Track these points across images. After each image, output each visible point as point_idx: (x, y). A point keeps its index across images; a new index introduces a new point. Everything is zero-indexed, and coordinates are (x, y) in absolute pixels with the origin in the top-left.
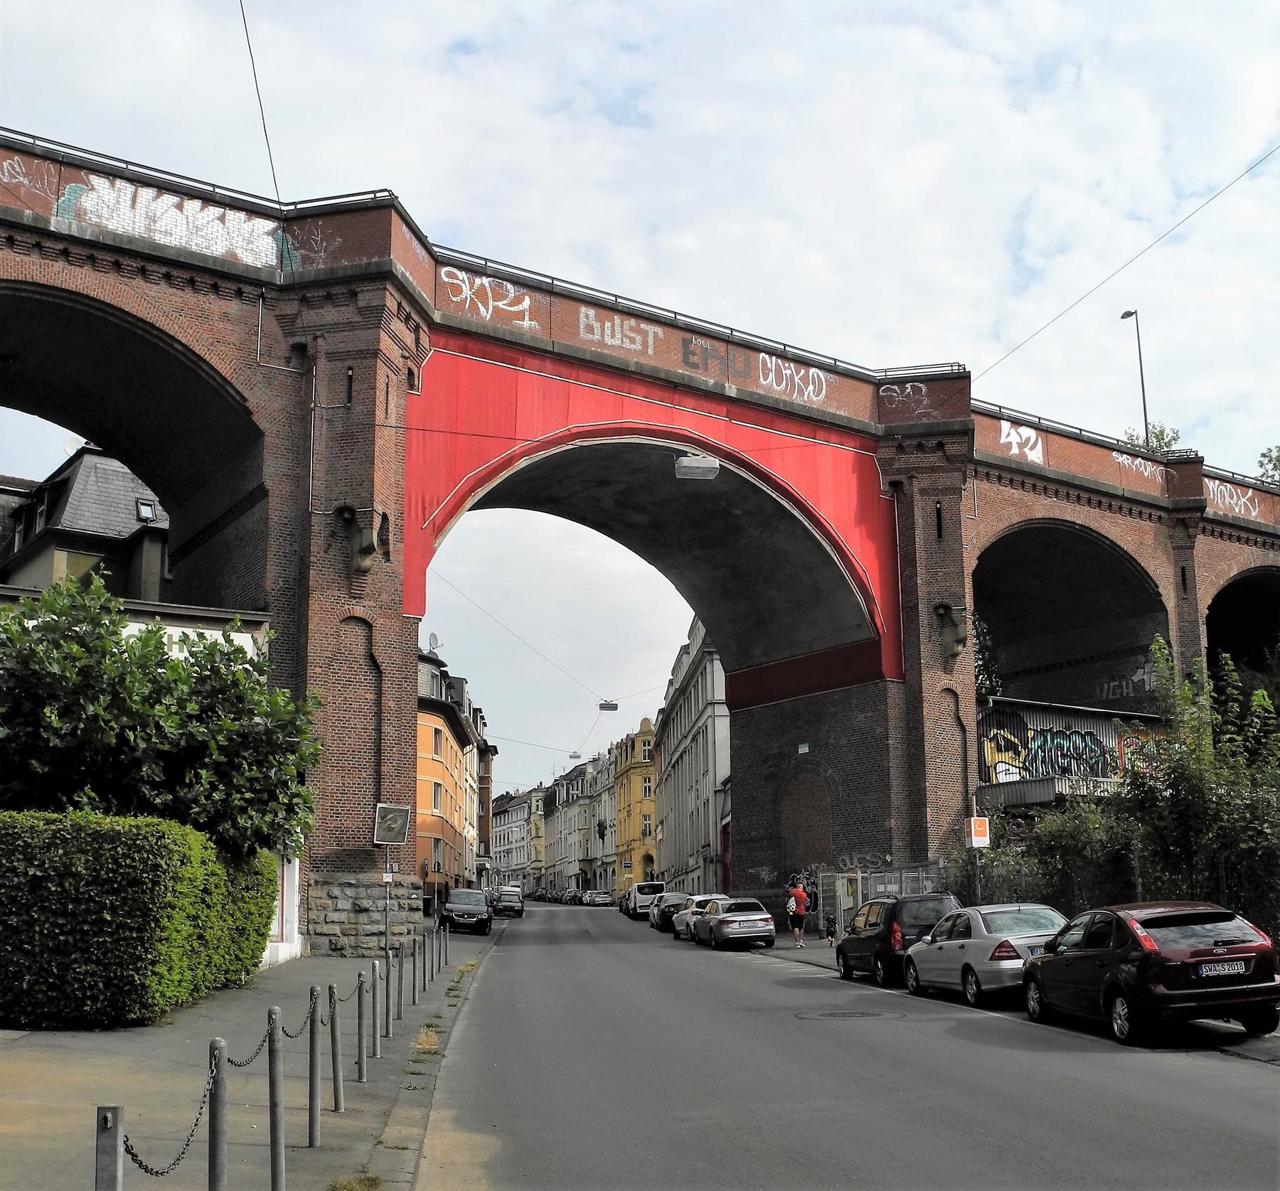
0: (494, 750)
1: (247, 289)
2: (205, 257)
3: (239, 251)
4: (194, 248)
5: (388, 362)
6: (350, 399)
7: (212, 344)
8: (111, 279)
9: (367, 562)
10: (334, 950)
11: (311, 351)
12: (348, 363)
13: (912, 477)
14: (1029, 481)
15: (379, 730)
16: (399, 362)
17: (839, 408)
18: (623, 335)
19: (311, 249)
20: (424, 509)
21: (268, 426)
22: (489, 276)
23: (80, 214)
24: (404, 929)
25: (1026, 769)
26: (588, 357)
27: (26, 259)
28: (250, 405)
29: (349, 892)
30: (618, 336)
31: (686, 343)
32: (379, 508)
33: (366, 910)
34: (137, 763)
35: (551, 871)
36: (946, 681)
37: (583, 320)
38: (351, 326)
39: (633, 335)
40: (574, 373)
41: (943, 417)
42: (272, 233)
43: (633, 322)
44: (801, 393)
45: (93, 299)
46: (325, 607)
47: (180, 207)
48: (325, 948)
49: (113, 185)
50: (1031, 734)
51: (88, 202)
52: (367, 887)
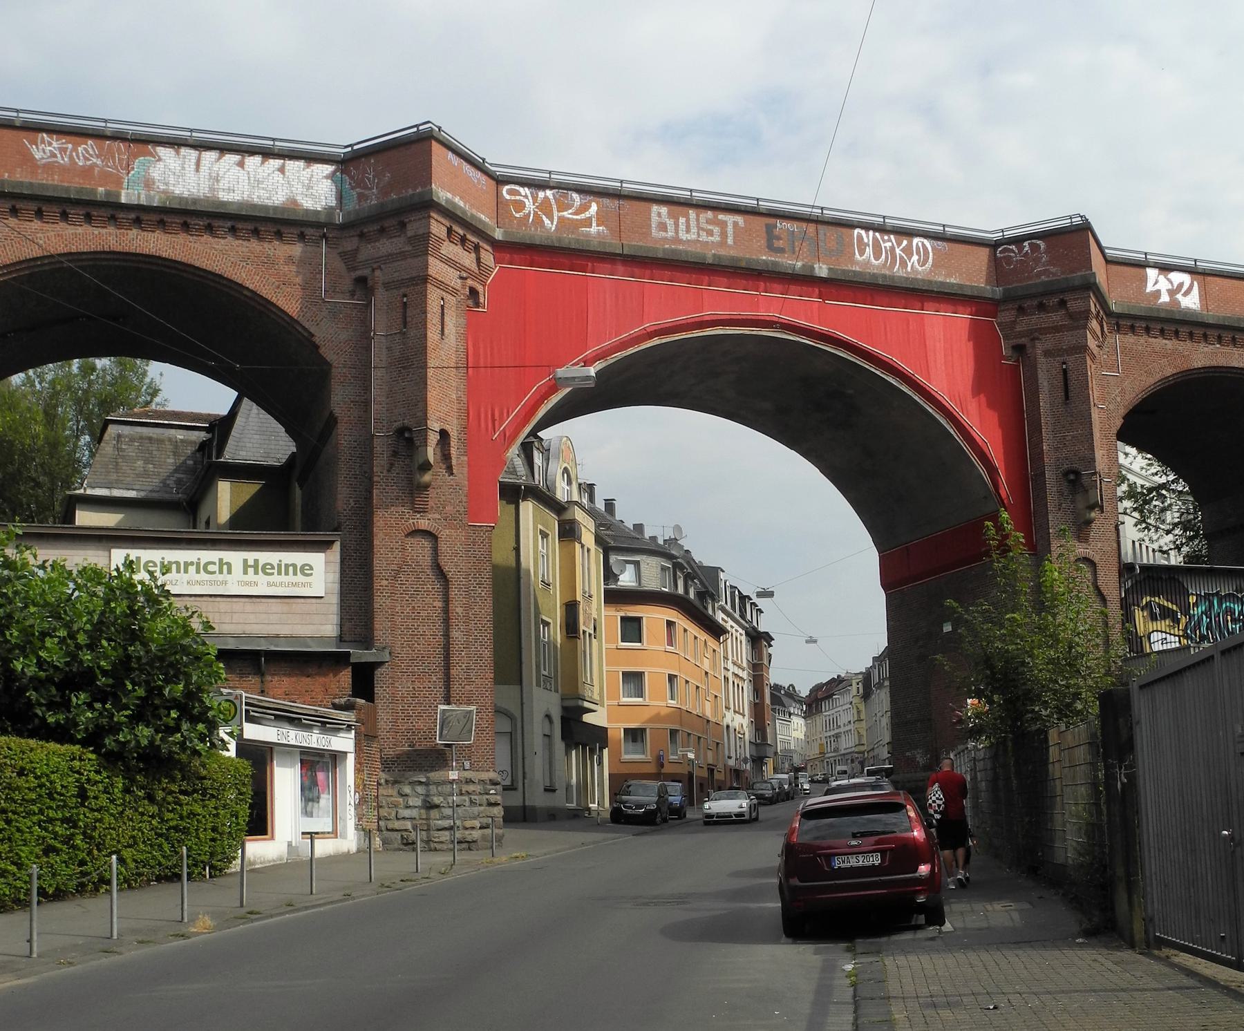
0: (768, 638)
1: (309, 231)
2: (266, 208)
3: (299, 198)
4: (256, 200)
5: (442, 285)
6: (405, 324)
7: (278, 287)
8: (182, 238)
9: (427, 478)
10: (407, 844)
11: (370, 283)
12: (403, 290)
13: (1033, 340)
14: (1184, 330)
15: (447, 635)
16: (457, 284)
17: (949, 275)
18: (699, 228)
19: (366, 188)
20: (494, 420)
21: (335, 357)
22: (552, 188)
23: (149, 184)
24: (477, 823)
25: (1187, 637)
26: (660, 255)
27: (104, 231)
28: (317, 340)
29: (420, 789)
30: (694, 230)
31: (770, 229)
32: (434, 425)
33: (437, 806)
34: (23, 690)
35: (871, 754)
36: (1081, 550)
37: (654, 219)
38: (403, 255)
39: (710, 227)
40: (648, 272)
41: (1063, 273)
42: (332, 176)
43: (710, 214)
44: (903, 264)
45: (165, 259)
46: (389, 525)
47: (241, 164)
48: (397, 843)
49: (178, 153)
50: (1192, 599)
51: (156, 172)
52: (438, 784)
